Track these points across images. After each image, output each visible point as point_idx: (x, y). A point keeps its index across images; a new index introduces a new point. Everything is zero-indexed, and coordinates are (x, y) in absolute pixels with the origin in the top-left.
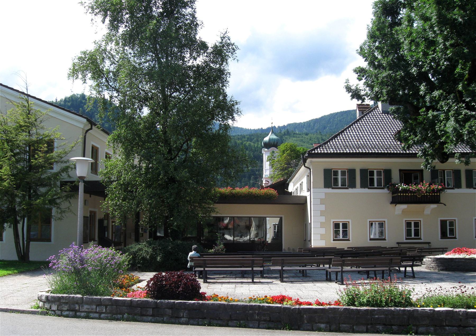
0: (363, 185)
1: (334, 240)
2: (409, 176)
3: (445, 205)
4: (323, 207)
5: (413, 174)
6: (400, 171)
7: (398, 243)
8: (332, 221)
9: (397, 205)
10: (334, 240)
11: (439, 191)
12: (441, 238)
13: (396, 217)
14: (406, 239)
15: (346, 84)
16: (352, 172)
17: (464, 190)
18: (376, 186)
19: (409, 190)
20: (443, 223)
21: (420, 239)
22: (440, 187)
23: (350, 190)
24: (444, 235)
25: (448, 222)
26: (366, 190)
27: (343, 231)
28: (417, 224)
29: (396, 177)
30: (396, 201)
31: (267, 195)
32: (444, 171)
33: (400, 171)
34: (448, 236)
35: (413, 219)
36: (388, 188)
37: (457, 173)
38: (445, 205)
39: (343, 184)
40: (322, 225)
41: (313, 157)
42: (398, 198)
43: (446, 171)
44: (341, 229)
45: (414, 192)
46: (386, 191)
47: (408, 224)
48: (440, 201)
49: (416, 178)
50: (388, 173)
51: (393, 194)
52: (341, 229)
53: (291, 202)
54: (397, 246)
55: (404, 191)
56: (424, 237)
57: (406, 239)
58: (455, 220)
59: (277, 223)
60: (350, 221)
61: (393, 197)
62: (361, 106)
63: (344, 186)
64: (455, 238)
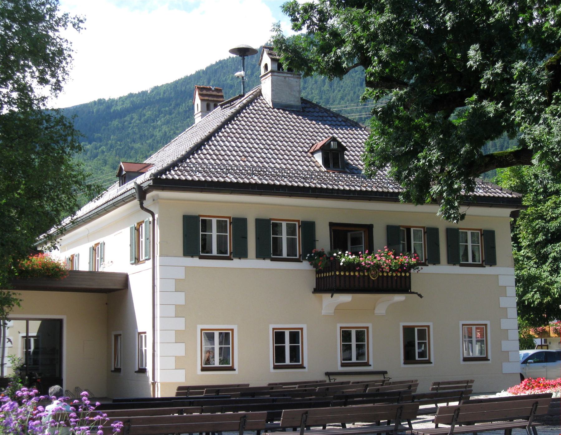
0: (261, 254)
1: (275, 367)
2: (346, 235)
3: (420, 296)
4: (180, 298)
5: (349, 234)
6: (331, 225)
7: (328, 374)
8: (271, 326)
9: (335, 295)
10: (203, 369)
11: (411, 266)
12: (405, 363)
13: (322, 320)
14: (343, 365)
15: (275, 34)
16: (239, 224)
17: (444, 269)
18: (285, 255)
19: (359, 264)
20: (408, 331)
21: (367, 364)
22: (413, 261)
23: (236, 263)
24: (409, 357)
25: (416, 329)
26: (267, 264)
27: (357, 346)
28: (361, 336)
29: (323, 240)
30: (323, 287)
31: (48, 269)
32: (408, 229)
33: (331, 225)
34: (417, 358)
35: (353, 324)
36: (311, 260)
37: (431, 234)
38: (420, 296)
39: (222, 249)
40: (180, 337)
41: (163, 189)
42: (330, 280)
43: (412, 229)
44: (354, 343)
45: (368, 270)
46: (305, 265)
47: (346, 335)
48: (410, 288)
49: (356, 241)
50: (308, 228)
51: (318, 272)
52: (354, 343)
53: (95, 286)
54: (326, 379)
55: (350, 266)
56: (375, 360)
57: (343, 365)
58: (428, 327)
59: (35, 334)
60: (235, 327)
61: (318, 280)
62: (205, 92)
63: (223, 255)
64: (429, 362)
